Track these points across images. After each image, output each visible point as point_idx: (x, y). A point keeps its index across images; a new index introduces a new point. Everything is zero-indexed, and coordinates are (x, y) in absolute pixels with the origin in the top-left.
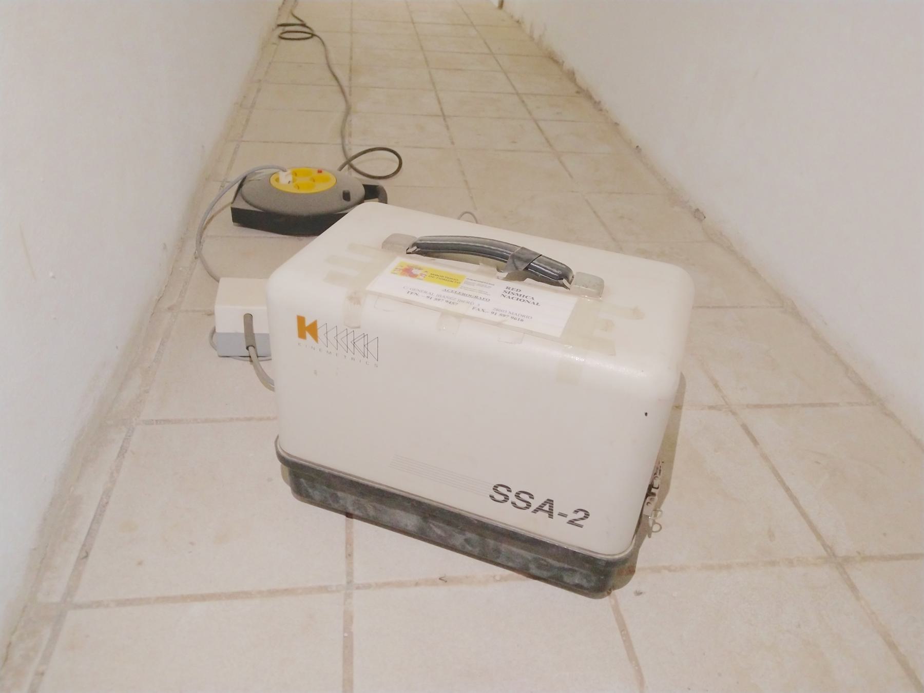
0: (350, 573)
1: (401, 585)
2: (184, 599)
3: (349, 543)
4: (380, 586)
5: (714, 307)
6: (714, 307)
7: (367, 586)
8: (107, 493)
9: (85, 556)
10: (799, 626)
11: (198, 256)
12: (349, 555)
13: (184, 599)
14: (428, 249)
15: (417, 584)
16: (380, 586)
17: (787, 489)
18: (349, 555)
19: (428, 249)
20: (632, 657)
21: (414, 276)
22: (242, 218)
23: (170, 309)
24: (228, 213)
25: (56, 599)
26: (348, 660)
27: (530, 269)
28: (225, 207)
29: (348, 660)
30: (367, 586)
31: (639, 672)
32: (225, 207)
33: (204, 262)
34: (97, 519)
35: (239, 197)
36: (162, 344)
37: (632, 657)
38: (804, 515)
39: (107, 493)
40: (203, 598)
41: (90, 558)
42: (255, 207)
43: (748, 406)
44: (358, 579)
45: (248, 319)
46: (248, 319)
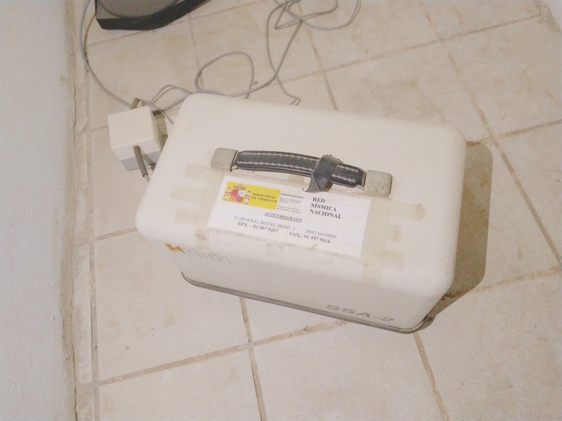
0: (249, 335)
1: (280, 338)
2: (159, 368)
3: (244, 312)
4: (270, 340)
5: (482, 30)
6: (482, 30)
7: (261, 342)
8: (93, 299)
9: (95, 348)
10: (536, 326)
11: (88, 69)
12: (246, 320)
13: (159, 368)
14: (246, 161)
15: (290, 336)
16: (270, 340)
17: (533, 211)
18: (246, 320)
19: (246, 161)
20: (427, 367)
21: (240, 200)
22: (106, 24)
23: (84, 129)
24: (96, 24)
25: (89, 380)
26: (258, 394)
27: (328, 174)
28: (92, 20)
29: (258, 394)
30: (261, 342)
31: (432, 376)
32: (92, 20)
33: (94, 76)
34: (93, 310)
35: (99, 7)
36: (89, 164)
37: (427, 367)
38: (544, 231)
39: (93, 299)
40: (168, 366)
41: (98, 347)
42: (114, 14)
43: (507, 134)
44: (255, 338)
45: (137, 149)
46: (137, 149)
